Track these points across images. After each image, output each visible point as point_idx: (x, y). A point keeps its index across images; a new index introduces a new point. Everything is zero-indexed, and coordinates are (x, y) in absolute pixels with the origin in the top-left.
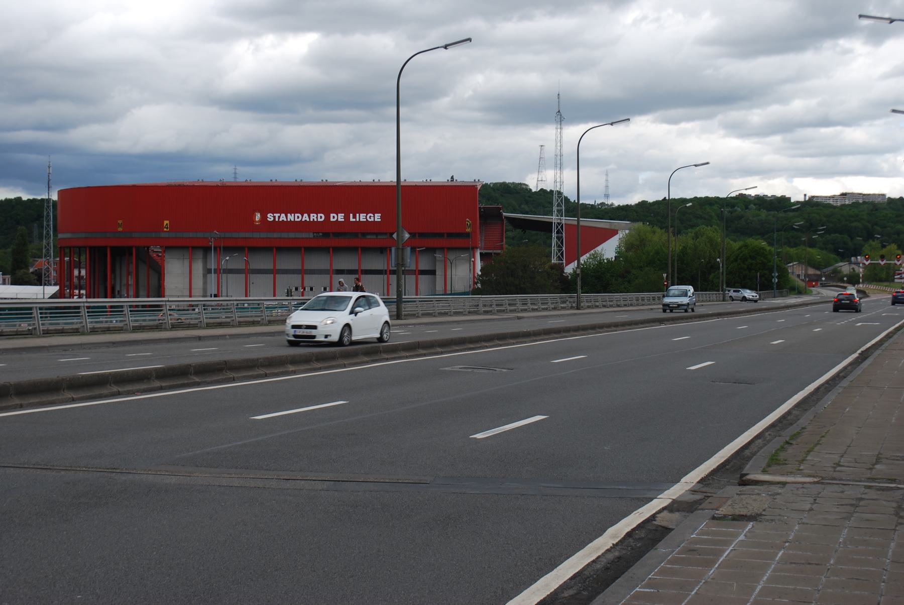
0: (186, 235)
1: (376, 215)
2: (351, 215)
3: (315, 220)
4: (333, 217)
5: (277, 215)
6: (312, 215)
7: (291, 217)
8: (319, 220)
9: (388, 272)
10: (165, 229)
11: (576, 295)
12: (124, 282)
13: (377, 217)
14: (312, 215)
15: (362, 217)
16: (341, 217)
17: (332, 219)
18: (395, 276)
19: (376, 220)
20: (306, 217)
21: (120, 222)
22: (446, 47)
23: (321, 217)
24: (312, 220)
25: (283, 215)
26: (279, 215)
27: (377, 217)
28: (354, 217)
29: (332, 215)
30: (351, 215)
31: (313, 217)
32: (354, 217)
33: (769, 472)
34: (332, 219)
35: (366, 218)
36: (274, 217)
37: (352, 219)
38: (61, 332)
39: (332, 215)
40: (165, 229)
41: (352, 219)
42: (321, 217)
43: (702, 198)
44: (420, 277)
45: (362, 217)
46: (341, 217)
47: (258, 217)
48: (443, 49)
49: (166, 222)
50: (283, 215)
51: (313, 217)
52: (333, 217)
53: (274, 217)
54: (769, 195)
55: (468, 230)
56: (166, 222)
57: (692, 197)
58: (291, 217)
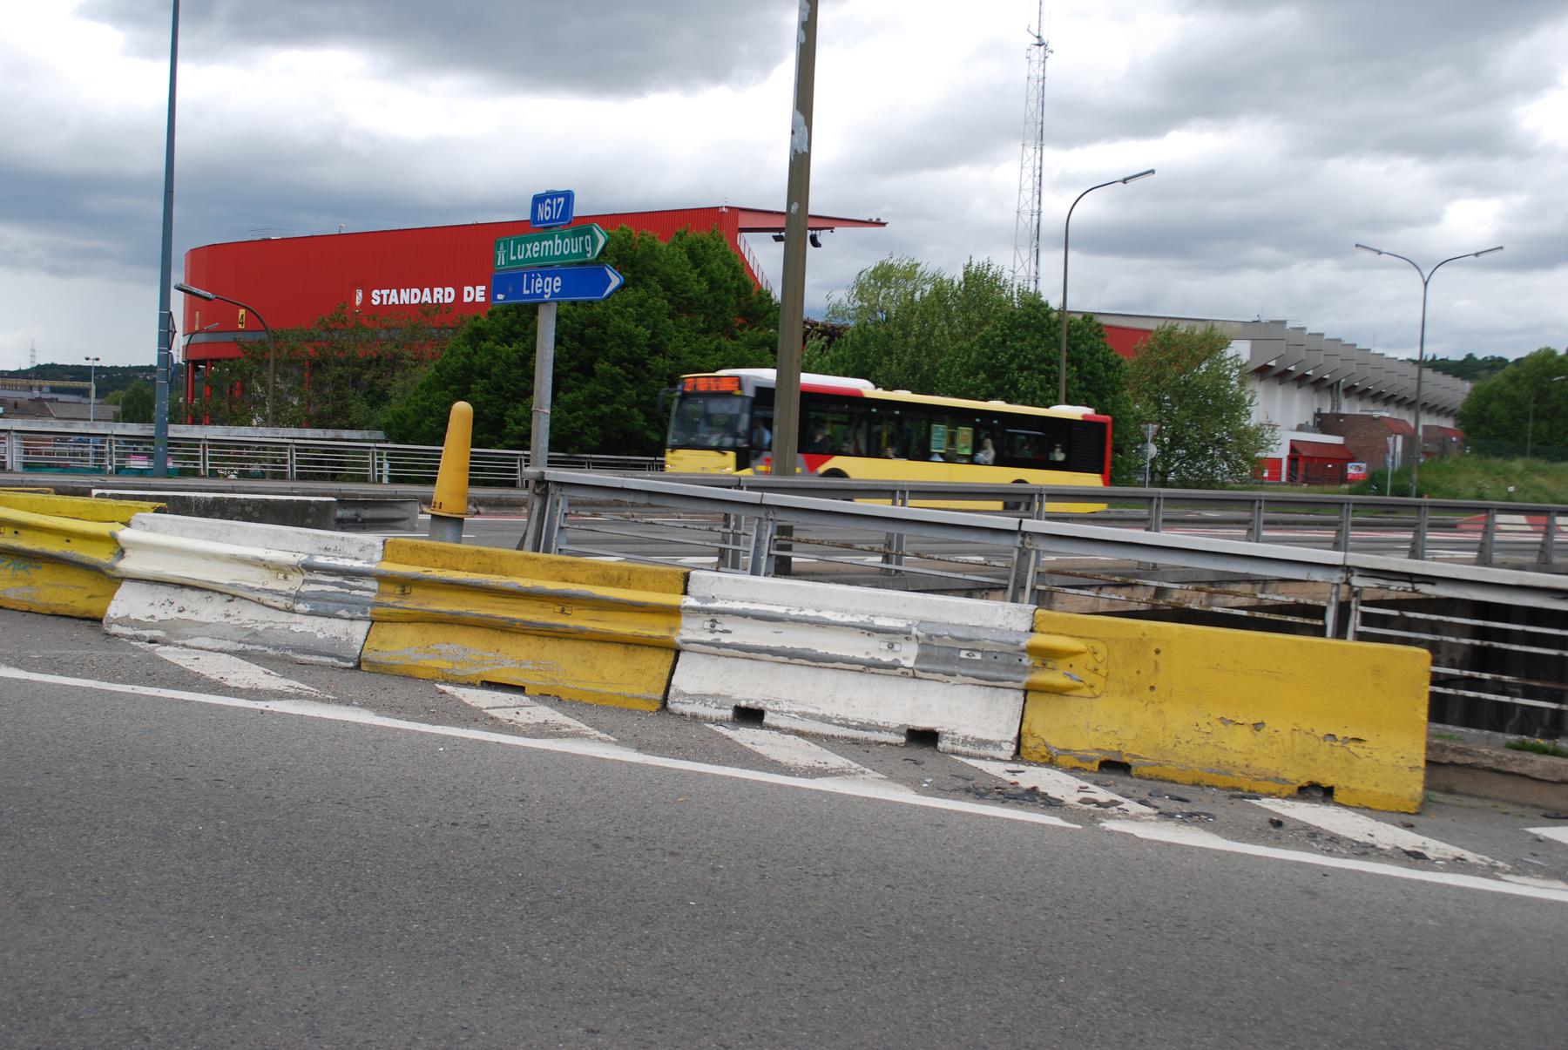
1: (478, 288)
3: (407, 302)
5: (385, 292)
6: (436, 290)
8: (448, 301)
10: (240, 326)
11: (1409, 536)
14: (436, 290)
19: (478, 299)
22: (1125, 181)
24: (435, 301)
25: (394, 292)
26: (388, 291)
29: (467, 289)
33: (1459, 528)
34: (467, 299)
35: (543, 288)
36: (381, 296)
38: (301, 492)
39: (467, 289)
40: (240, 326)
43: (67, 366)
47: (359, 294)
48: (1121, 184)
50: (394, 292)
53: (381, 296)
57: (148, 365)
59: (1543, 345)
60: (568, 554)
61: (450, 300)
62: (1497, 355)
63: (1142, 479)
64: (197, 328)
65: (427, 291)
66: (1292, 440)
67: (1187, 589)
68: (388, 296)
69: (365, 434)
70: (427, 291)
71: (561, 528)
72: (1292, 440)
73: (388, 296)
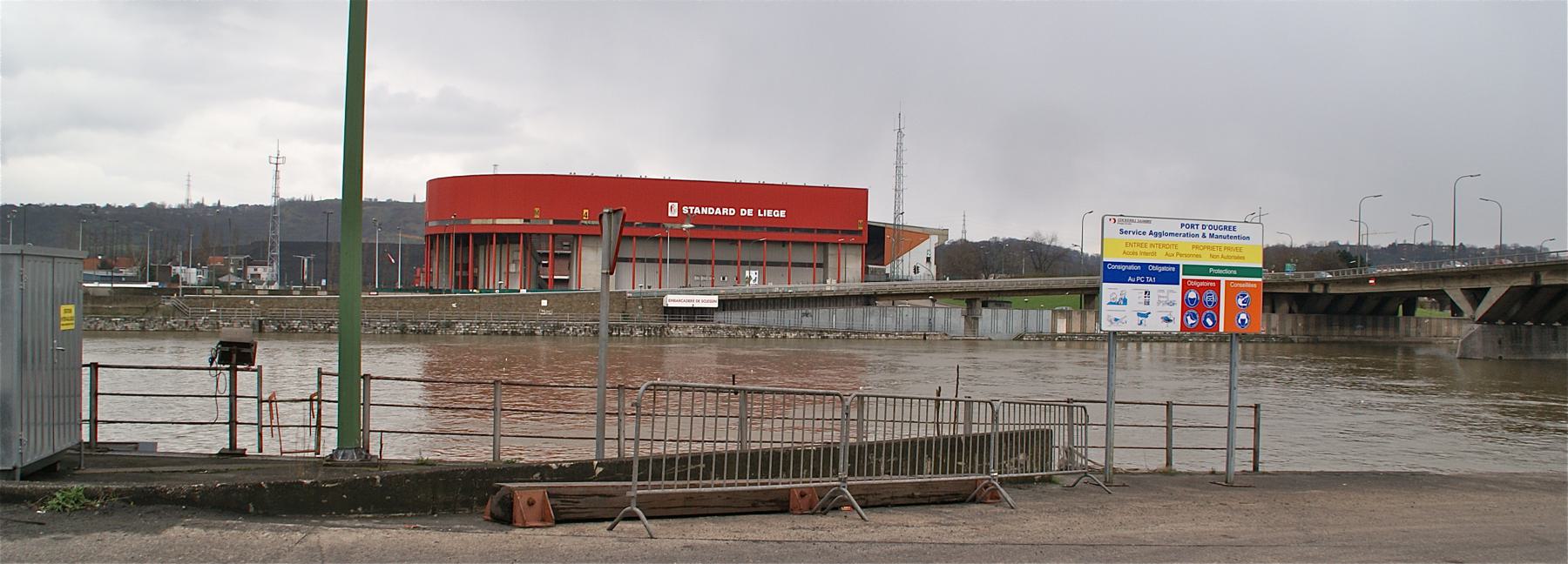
0: (499, 221)
2: (759, 211)
4: (743, 212)
5: (692, 208)
6: (724, 209)
7: (704, 211)
8: (730, 214)
9: (634, 260)
11: (555, 277)
12: (504, 270)
13: (782, 214)
14: (724, 209)
15: (769, 213)
16: (750, 212)
17: (742, 214)
18: (822, 269)
19: (749, 215)
20: (718, 211)
21: (537, 209)
23: (732, 212)
25: (697, 208)
27: (782, 214)
28: (762, 213)
29: (742, 210)
30: (759, 211)
31: (725, 211)
32: (762, 213)
34: (742, 214)
36: (689, 210)
37: (760, 215)
39: (742, 210)
41: (760, 215)
42: (732, 212)
44: (637, 264)
45: (769, 213)
46: (750, 212)
49: (585, 211)
50: (697, 208)
51: (725, 211)
52: (743, 212)
53: (689, 210)
54: (158, 203)
55: (860, 228)
56: (585, 211)
58: (704, 211)
59: (149, 202)
60: (703, 487)
61: (733, 214)
62: (54, 203)
63: (1214, 300)
64: (598, 223)
65: (718, 209)
66: (865, 191)
67: (1006, 513)
68: (694, 210)
69: (1066, 440)
70: (718, 209)
71: (820, 498)
72: (865, 191)
73: (694, 210)
